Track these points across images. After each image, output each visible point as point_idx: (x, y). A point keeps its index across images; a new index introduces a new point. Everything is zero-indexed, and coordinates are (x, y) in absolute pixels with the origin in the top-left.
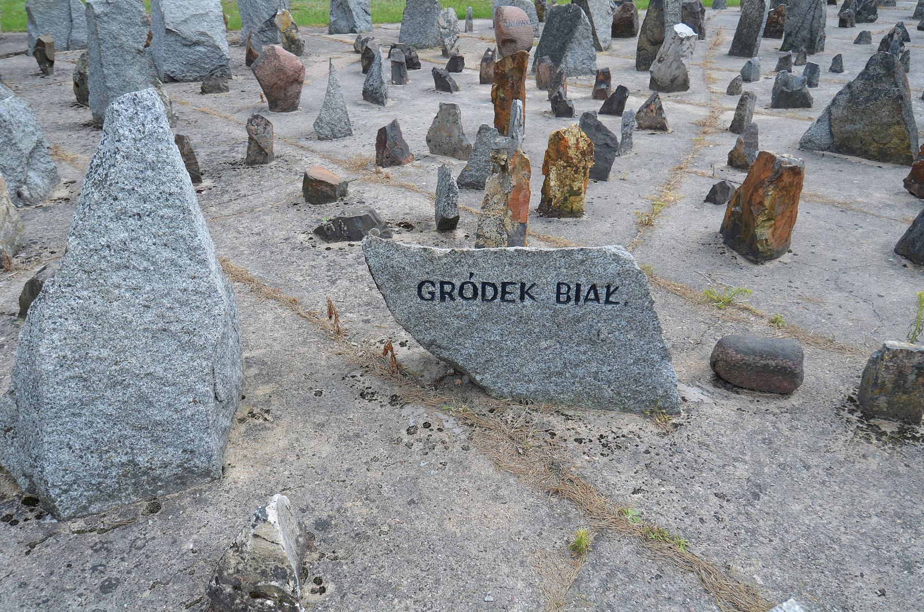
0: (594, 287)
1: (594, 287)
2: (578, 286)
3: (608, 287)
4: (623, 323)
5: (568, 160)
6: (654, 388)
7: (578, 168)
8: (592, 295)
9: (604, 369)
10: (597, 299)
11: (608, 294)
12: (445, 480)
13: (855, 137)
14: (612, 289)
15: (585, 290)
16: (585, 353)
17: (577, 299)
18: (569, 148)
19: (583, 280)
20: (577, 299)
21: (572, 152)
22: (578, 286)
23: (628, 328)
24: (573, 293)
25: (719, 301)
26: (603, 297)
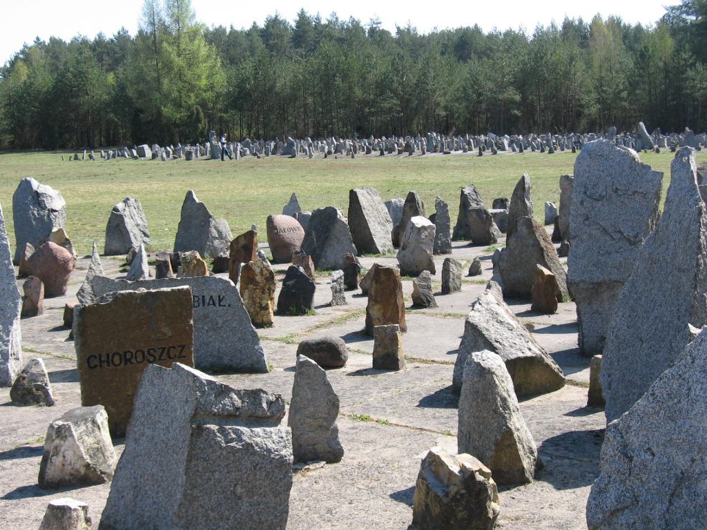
0: (211, 297)
1: (211, 297)
2: (203, 297)
3: (219, 297)
4: (230, 317)
5: (256, 283)
6: (251, 356)
7: (264, 290)
8: (211, 303)
9: (223, 346)
10: (214, 304)
11: (220, 301)
12: (88, 227)
13: (240, 87)
14: (221, 298)
15: (207, 299)
16: (211, 336)
17: (204, 305)
18: (257, 275)
19: (205, 293)
20: (204, 305)
21: (258, 278)
22: (203, 297)
23: (233, 320)
24: (201, 301)
25: (405, 435)
26: (217, 302)
